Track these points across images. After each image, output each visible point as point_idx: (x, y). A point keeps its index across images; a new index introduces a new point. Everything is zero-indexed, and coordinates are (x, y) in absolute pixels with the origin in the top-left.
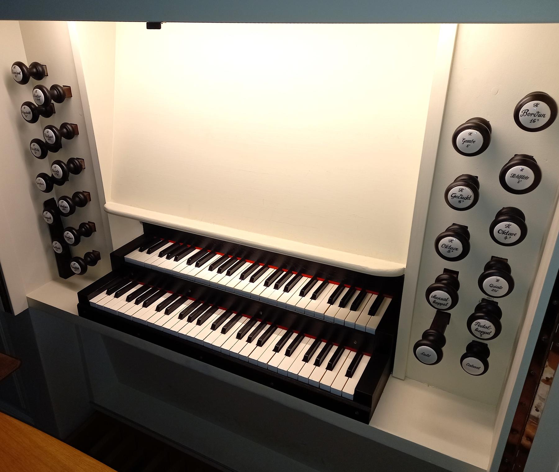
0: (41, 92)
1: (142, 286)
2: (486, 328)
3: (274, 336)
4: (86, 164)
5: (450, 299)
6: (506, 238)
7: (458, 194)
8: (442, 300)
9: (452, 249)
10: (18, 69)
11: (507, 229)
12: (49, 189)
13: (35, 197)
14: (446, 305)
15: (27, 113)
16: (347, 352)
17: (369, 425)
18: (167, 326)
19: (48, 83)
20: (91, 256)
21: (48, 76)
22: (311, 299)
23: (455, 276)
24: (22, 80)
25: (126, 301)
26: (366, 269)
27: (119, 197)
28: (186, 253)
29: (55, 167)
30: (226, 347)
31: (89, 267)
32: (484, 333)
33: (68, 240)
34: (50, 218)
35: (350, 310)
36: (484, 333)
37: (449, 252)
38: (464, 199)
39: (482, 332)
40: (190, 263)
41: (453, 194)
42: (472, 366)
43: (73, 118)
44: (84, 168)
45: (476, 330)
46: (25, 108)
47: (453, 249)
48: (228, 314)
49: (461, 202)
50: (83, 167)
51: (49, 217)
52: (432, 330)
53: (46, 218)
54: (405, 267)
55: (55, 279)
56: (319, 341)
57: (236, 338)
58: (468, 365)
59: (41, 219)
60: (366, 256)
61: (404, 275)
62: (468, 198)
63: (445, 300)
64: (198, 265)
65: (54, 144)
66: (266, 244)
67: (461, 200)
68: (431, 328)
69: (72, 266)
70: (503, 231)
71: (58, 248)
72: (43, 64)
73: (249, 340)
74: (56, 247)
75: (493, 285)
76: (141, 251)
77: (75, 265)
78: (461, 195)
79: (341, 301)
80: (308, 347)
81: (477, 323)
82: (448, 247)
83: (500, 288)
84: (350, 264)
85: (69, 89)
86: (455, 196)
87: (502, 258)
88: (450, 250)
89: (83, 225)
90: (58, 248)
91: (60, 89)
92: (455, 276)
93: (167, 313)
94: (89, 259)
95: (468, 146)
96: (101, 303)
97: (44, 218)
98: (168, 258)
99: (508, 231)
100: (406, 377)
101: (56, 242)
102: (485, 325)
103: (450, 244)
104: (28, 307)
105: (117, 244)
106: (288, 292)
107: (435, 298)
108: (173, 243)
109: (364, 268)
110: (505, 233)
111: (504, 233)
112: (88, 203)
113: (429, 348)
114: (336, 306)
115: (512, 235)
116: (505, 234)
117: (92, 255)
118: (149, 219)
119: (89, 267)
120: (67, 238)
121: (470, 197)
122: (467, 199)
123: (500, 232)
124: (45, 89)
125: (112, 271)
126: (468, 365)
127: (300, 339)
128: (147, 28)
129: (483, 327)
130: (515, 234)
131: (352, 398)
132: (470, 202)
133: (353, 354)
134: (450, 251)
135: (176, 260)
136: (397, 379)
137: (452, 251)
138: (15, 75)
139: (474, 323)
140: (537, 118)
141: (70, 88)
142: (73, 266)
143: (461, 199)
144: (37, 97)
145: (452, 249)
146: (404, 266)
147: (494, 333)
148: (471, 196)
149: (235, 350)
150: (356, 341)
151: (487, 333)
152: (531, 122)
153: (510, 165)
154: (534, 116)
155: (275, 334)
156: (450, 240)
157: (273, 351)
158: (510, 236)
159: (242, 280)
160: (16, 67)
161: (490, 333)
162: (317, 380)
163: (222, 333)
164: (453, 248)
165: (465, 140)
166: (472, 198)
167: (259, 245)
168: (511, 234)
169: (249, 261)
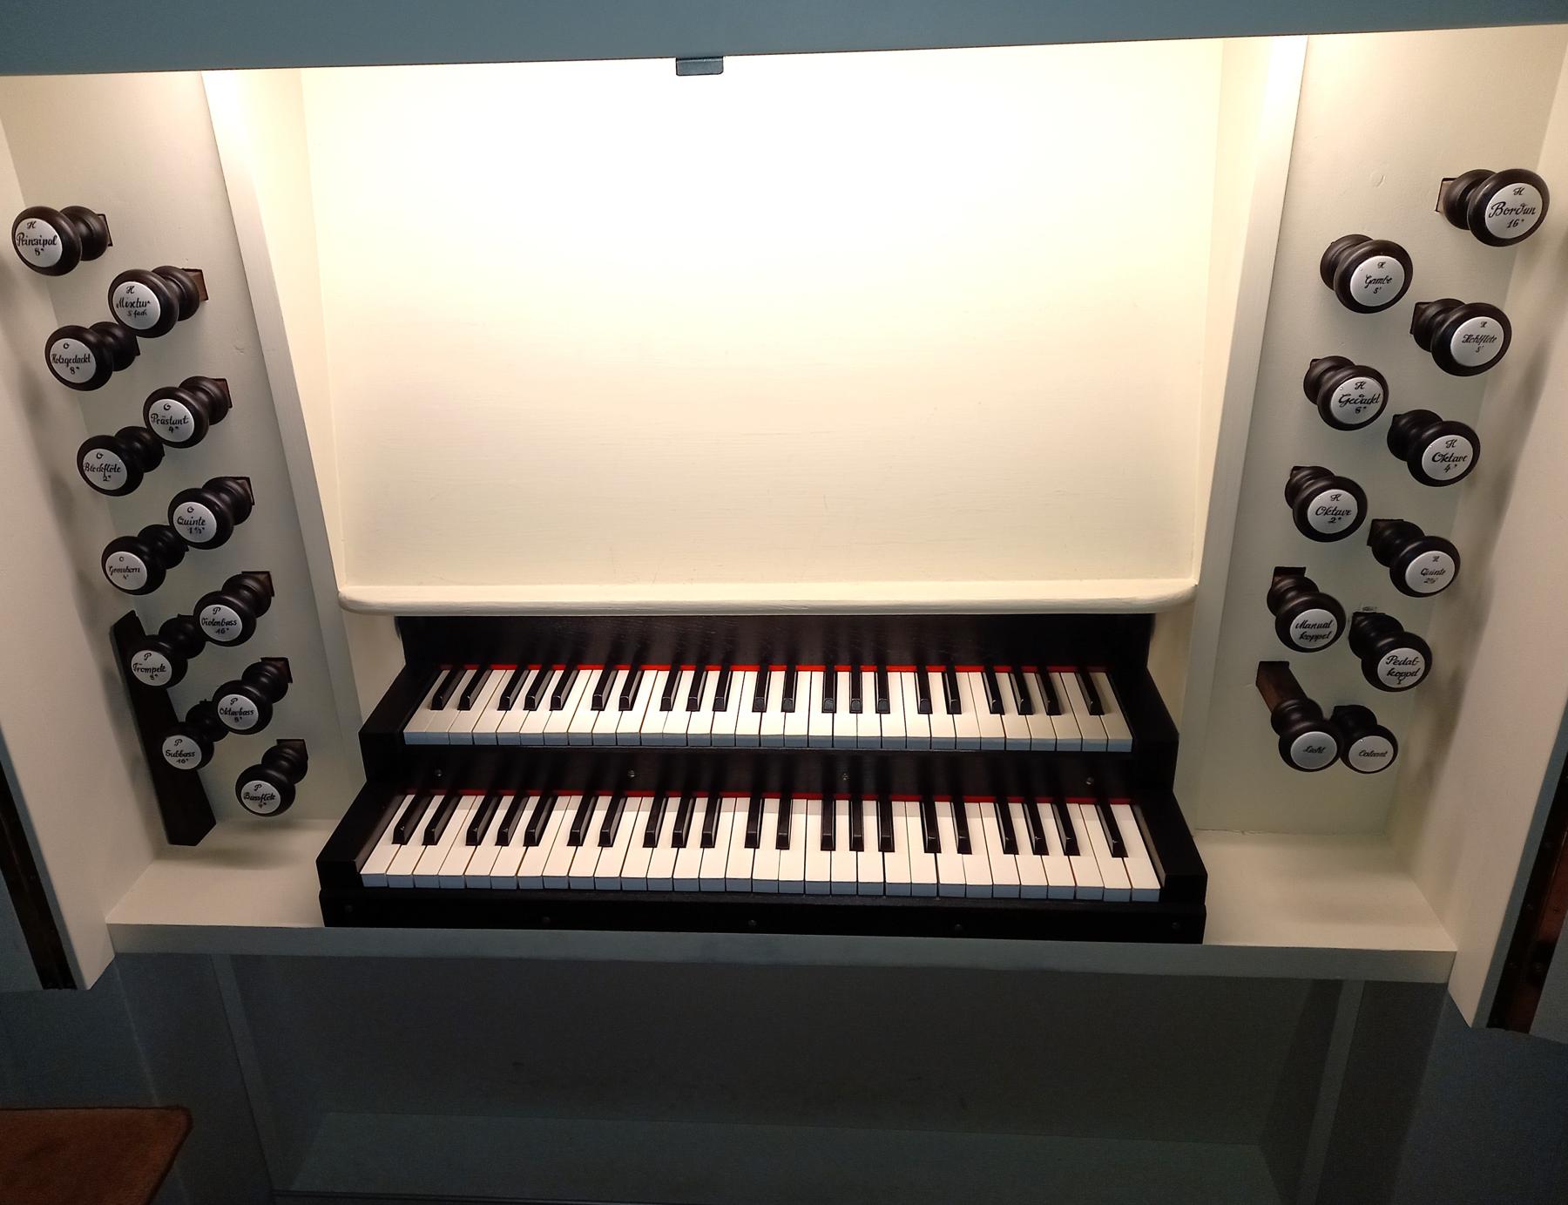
1: (414, 796)
3: (556, 815)
5: (1335, 622)
6: (1447, 469)
7: (1355, 395)
15: (77, 360)
29: (190, 510)
32: (1406, 675)
34: (162, 668)
41: (1344, 396)
42: (1372, 754)
45: (1390, 673)
48: (423, 803)
52: (1286, 701)
53: (147, 670)
56: (548, 798)
71: (186, 755)
80: (571, 815)
86: (1348, 401)
111: (1444, 460)
127: (547, 807)
129: (1404, 663)
133: (744, 802)
138: (35, 247)
142: (253, 794)
151: (1412, 674)
154: (1516, 213)
155: (867, 815)
162: (485, 873)
168: (1458, 459)
169: (584, 666)
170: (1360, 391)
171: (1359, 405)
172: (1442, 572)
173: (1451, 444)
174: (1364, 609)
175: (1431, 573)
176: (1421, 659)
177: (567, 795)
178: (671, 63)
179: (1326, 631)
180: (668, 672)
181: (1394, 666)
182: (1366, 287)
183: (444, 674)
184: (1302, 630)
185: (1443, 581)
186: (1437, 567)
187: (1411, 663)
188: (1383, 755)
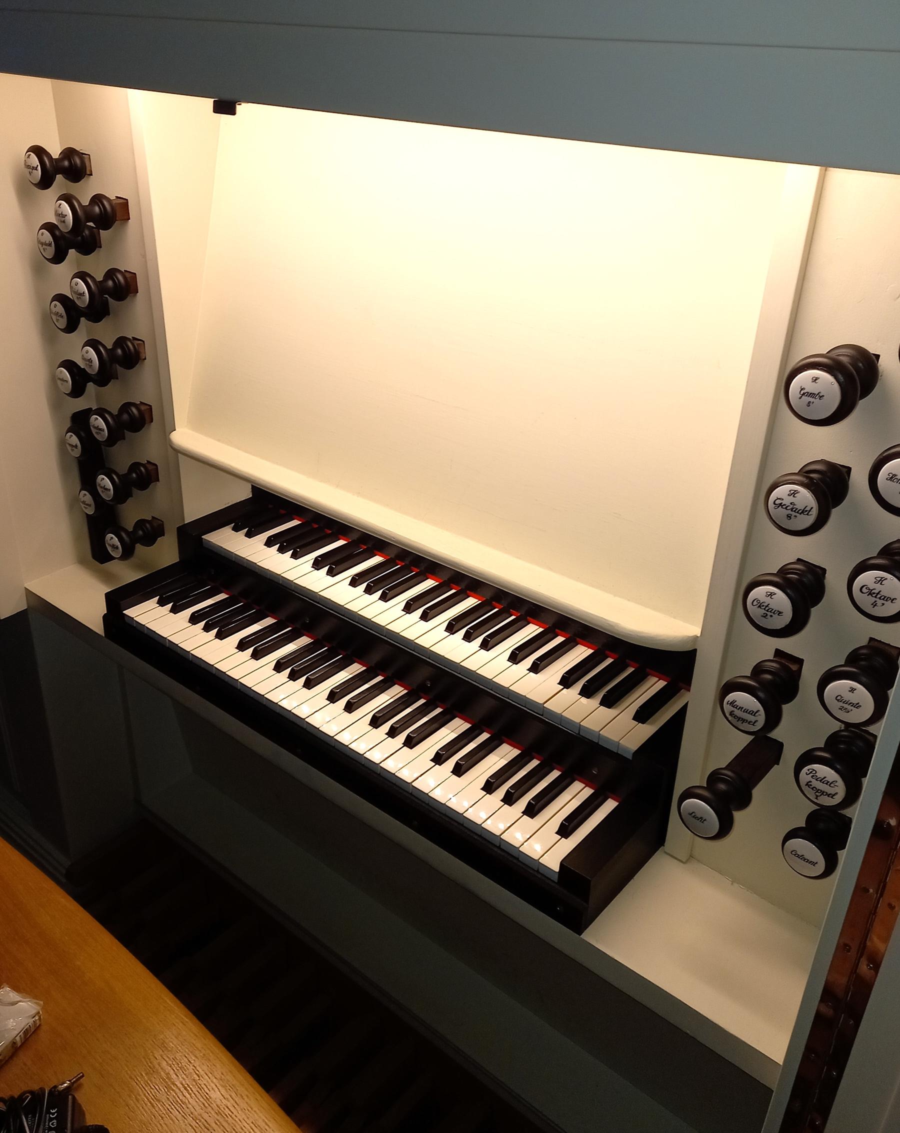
0: (68, 208)
2: (827, 784)
4: (148, 352)
6: (874, 605)
7: (787, 501)
8: (746, 712)
9: (770, 612)
10: (34, 160)
11: (878, 587)
12: (77, 391)
13: (56, 405)
14: (753, 725)
15: (46, 245)
16: (577, 786)
17: (581, 936)
18: (248, 682)
19: (85, 193)
20: (146, 527)
21: (91, 175)
22: (528, 670)
23: (794, 667)
24: (39, 182)
25: (189, 622)
26: (616, 628)
27: (200, 423)
28: (316, 545)
30: (345, 738)
31: (139, 547)
32: (823, 793)
33: (102, 491)
34: (76, 446)
35: (599, 704)
36: (822, 794)
37: (765, 616)
38: (798, 512)
39: (818, 791)
40: (317, 566)
41: (778, 499)
42: (802, 857)
43: (129, 263)
44: (144, 358)
46: (42, 234)
47: (773, 611)
49: (790, 519)
50: (141, 355)
51: (74, 444)
53: (70, 445)
54: (699, 635)
55: (82, 561)
57: (369, 725)
58: (793, 853)
59: (62, 445)
60: (629, 600)
61: (695, 650)
62: (806, 511)
63: (751, 714)
64: (331, 573)
65: (86, 307)
66: (439, 550)
67: (791, 513)
68: (728, 767)
69: (107, 540)
70: (869, 589)
71: (87, 505)
72: (86, 151)
73: (392, 733)
74: (84, 502)
75: (842, 697)
76: (236, 529)
77: (112, 539)
78: (791, 503)
79: (584, 684)
81: (811, 770)
82: (763, 606)
83: (857, 706)
84: (587, 612)
85: (124, 204)
87: (889, 645)
89: (135, 466)
90: (87, 505)
91: (105, 203)
92: (794, 667)
93: (256, 656)
94: (141, 533)
95: (809, 404)
96: (141, 620)
97: (68, 446)
98: (282, 550)
99: (880, 591)
100: (691, 856)
101: (86, 492)
102: (825, 777)
103: (768, 600)
104: (26, 608)
105: (194, 510)
106: (488, 651)
107: (734, 707)
108: (300, 522)
109: (612, 624)
110: (874, 593)
112: (146, 425)
113: (709, 807)
114: (573, 692)
115: (886, 600)
116: (874, 595)
117: (148, 525)
118: (240, 471)
119: (139, 547)
120: (101, 487)
121: (810, 511)
123: (864, 590)
124: (77, 202)
125: (178, 560)
128: (214, 112)
129: (822, 780)
130: (894, 599)
131: (555, 878)
132: (808, 521)
135: (295, 556)
136: (672, 859)
137: (771, 616)
138: (29, 170)
139: (805, 770)
141: (128, 202)
143: (792, 511)
144: (61, 216)
145: (770, 612)
147: (843, 797)
148: (812, 508)
149: (359, 747)
150: (596, 769)
153: (889, 454)
156: (769, 594)
157: (431, 760)
159: (407, 613)
160: (31, 156)
161: (834, 795)
163: (346, 711)
164: (773, 610)
165: (805, 391)
166: (814, 513)
167: (425, 548)
168: (886, 599)
169: (433, 577)
170: (791, 499)
171: (790, 512)
177: (464, 720)
178: (209, 103)
181: (812, 780)
182: (800, 398)
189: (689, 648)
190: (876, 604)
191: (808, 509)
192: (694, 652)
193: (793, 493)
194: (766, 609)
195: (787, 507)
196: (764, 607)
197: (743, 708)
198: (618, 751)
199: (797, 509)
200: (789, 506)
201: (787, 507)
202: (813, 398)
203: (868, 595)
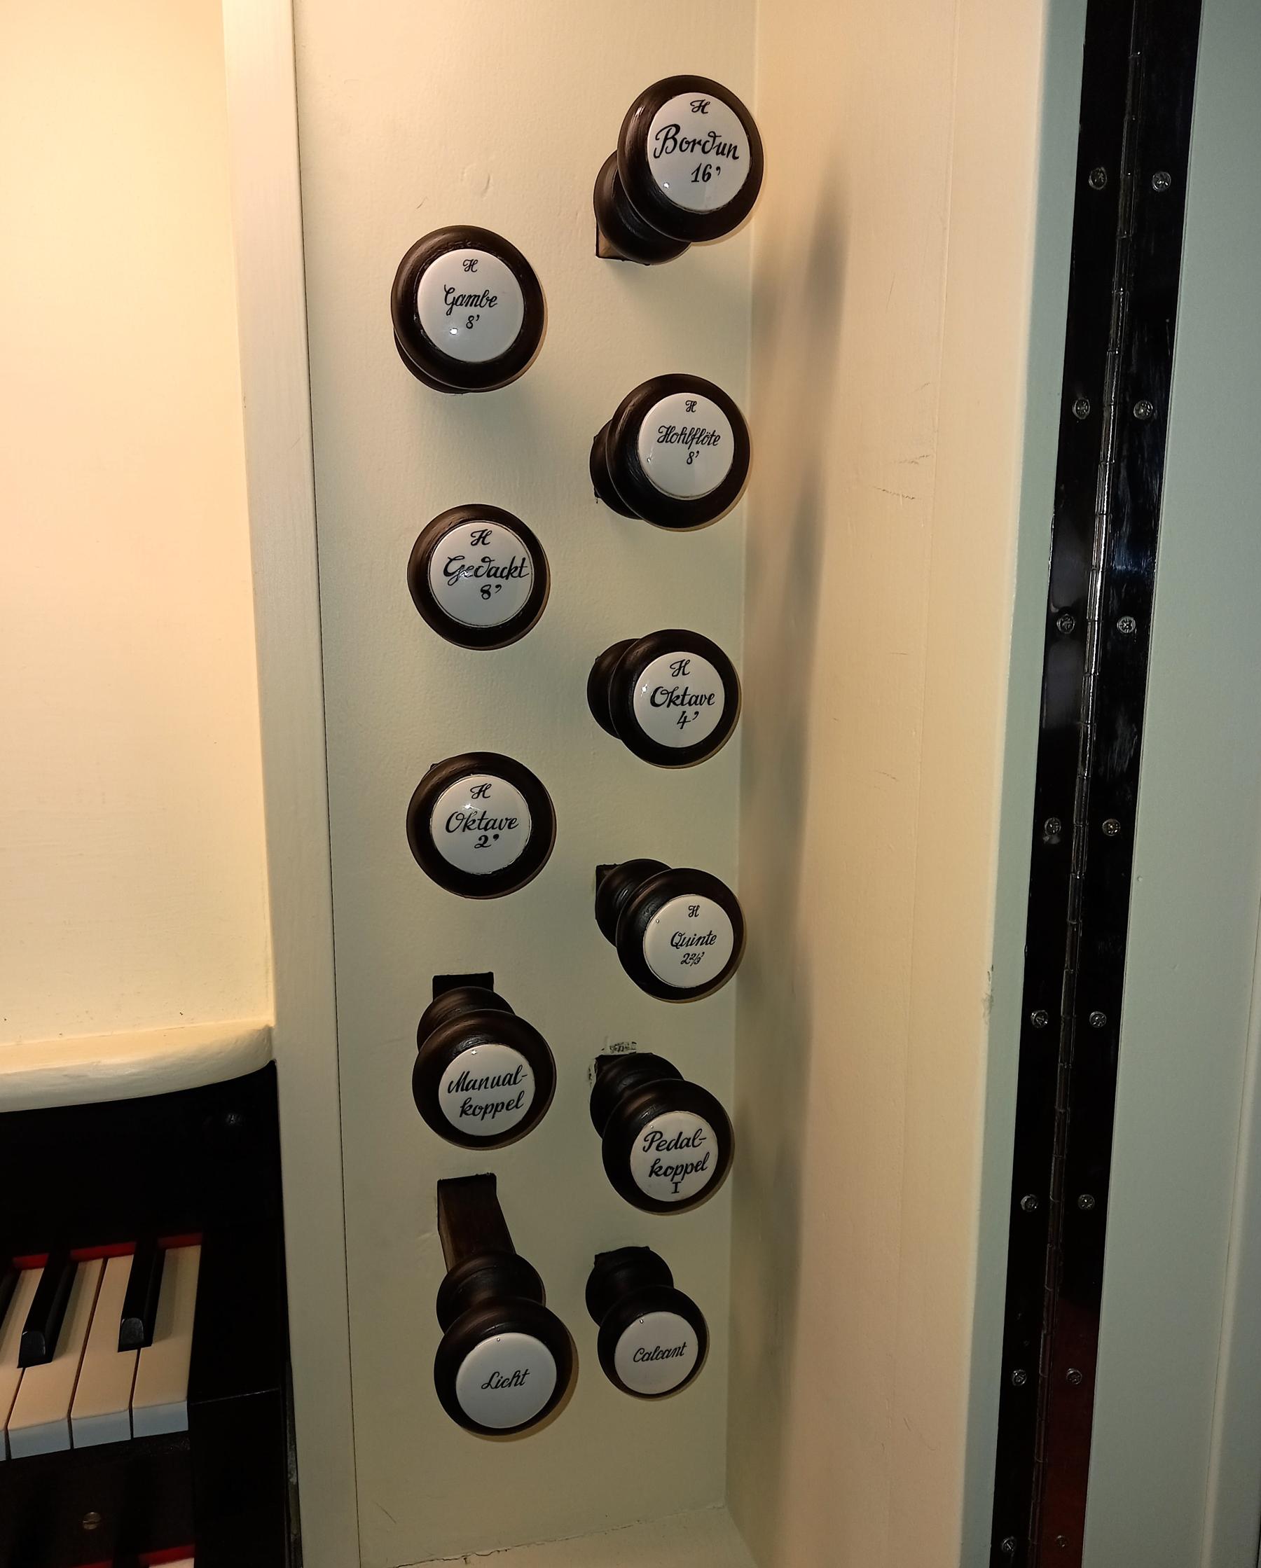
2: (687, 1145)
5: (527, 1069)
6: (683, 721)
7: (474, 556)
8: (498, 1084)
14: (516, 1106)
38: (501, 576)
41: (451, 560)
42: (660, 1354)
47: (497, 825)
49: (489, 594)
52: (469, 1260)
54: (272, 1023)
61: (271, 1069)
70: (668, 693)
78: (483, 560)
81: (650, 1138)
82: (474, 821)
88: (486, 833)
122: (510, 573)
123: (659, 698)
126: (639, 1356)
129: (678, 1144)
134: (486, 838)
139: (639, 1143)
140: (713, 159)
143: (489, 576)
145: (492, 827)
146: (266, 1016)
148: (524, 559)
152: (696, 180)
158: (694, 708)
165: (456, 294)
171: (485, 580)
172: (709, 940)
173: (681, 668)
174: (614, 1048)
175: (690, 943)
176: (708, 1131)
179: (505, 1093)
180: (133, 1256)
183: (32, 1281)
184: (462, 1096)
185: (716, 958)
186: (697, 927)
187: (690, 1143)
188: (679, 1351)
189: (261, 1063)
190: (686, 717)
191: (518, 563)
192: (268, 1074)
193: (480, 537)
194: (481, 827)
195: (477, 569)
196: (477, 822)
197: (487, 1079)
198: (184, 1401)
199: (498, 568)
200: (480, 567)
201: (477, 569)
202: (476, 306)
203: (668, 706)
